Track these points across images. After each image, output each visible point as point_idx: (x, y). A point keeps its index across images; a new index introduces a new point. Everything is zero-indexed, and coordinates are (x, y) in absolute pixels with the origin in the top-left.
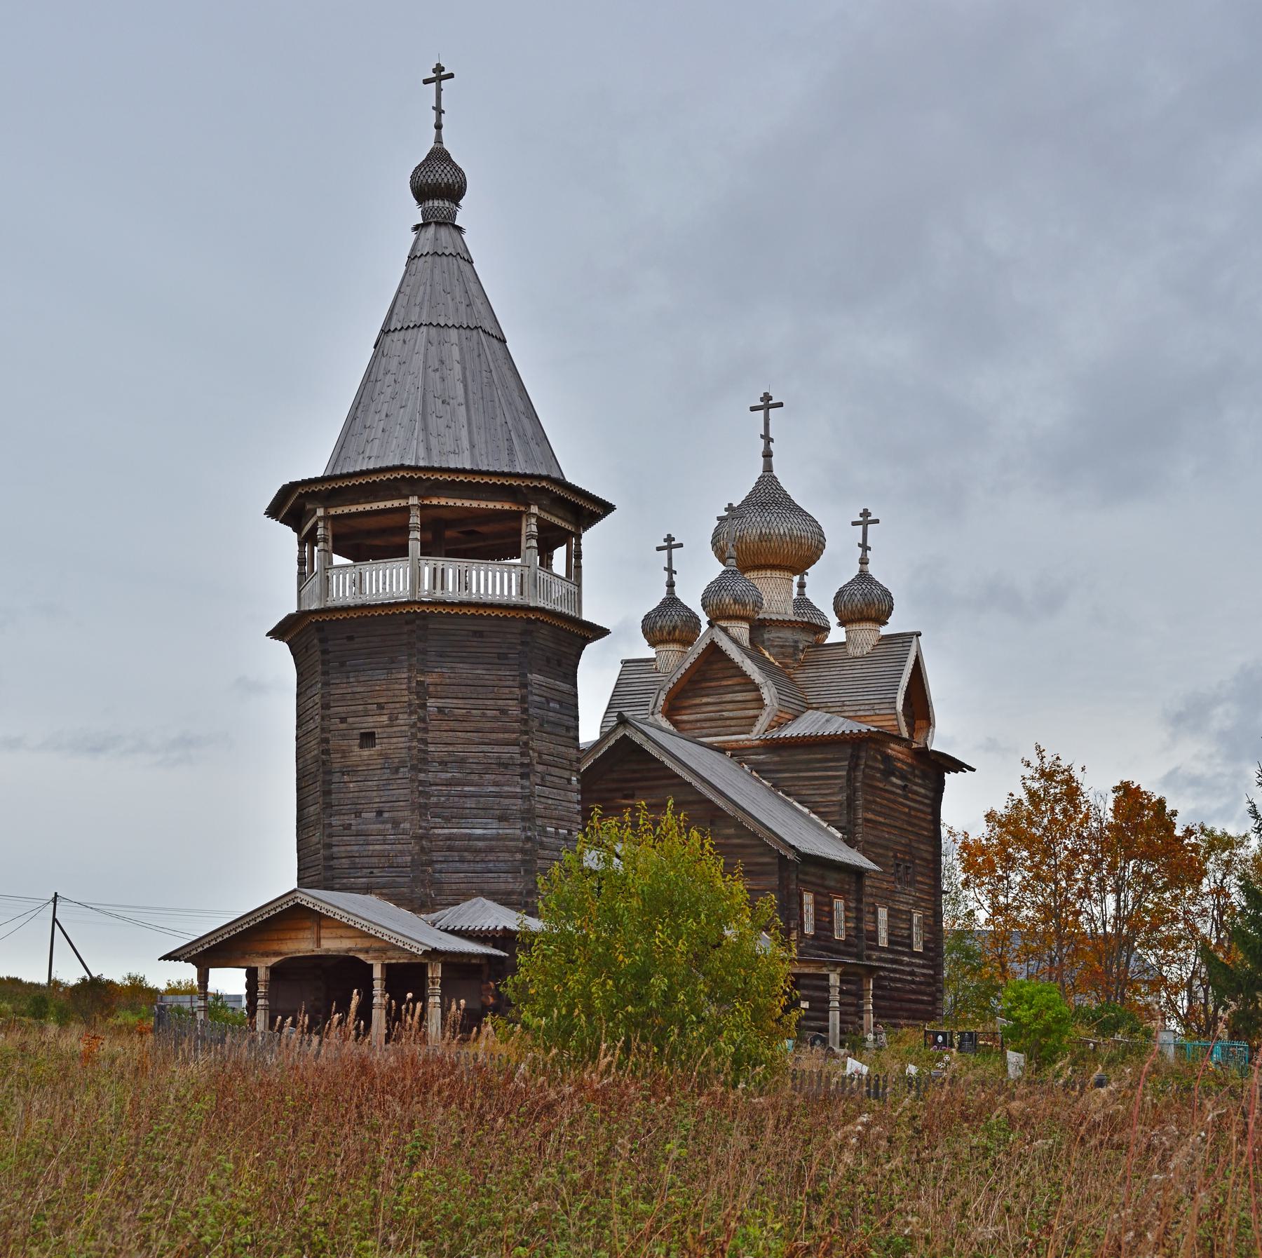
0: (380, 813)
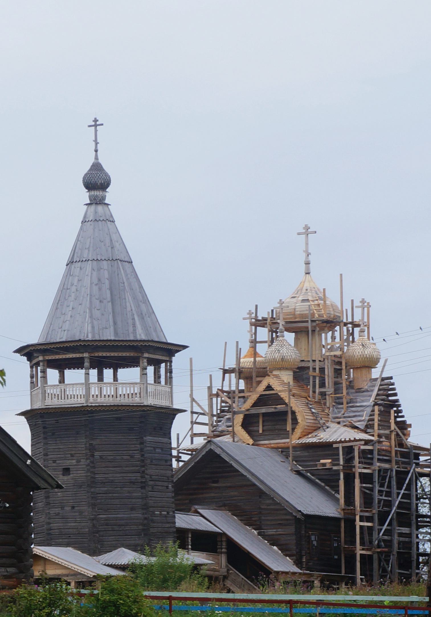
0: (73, 507)
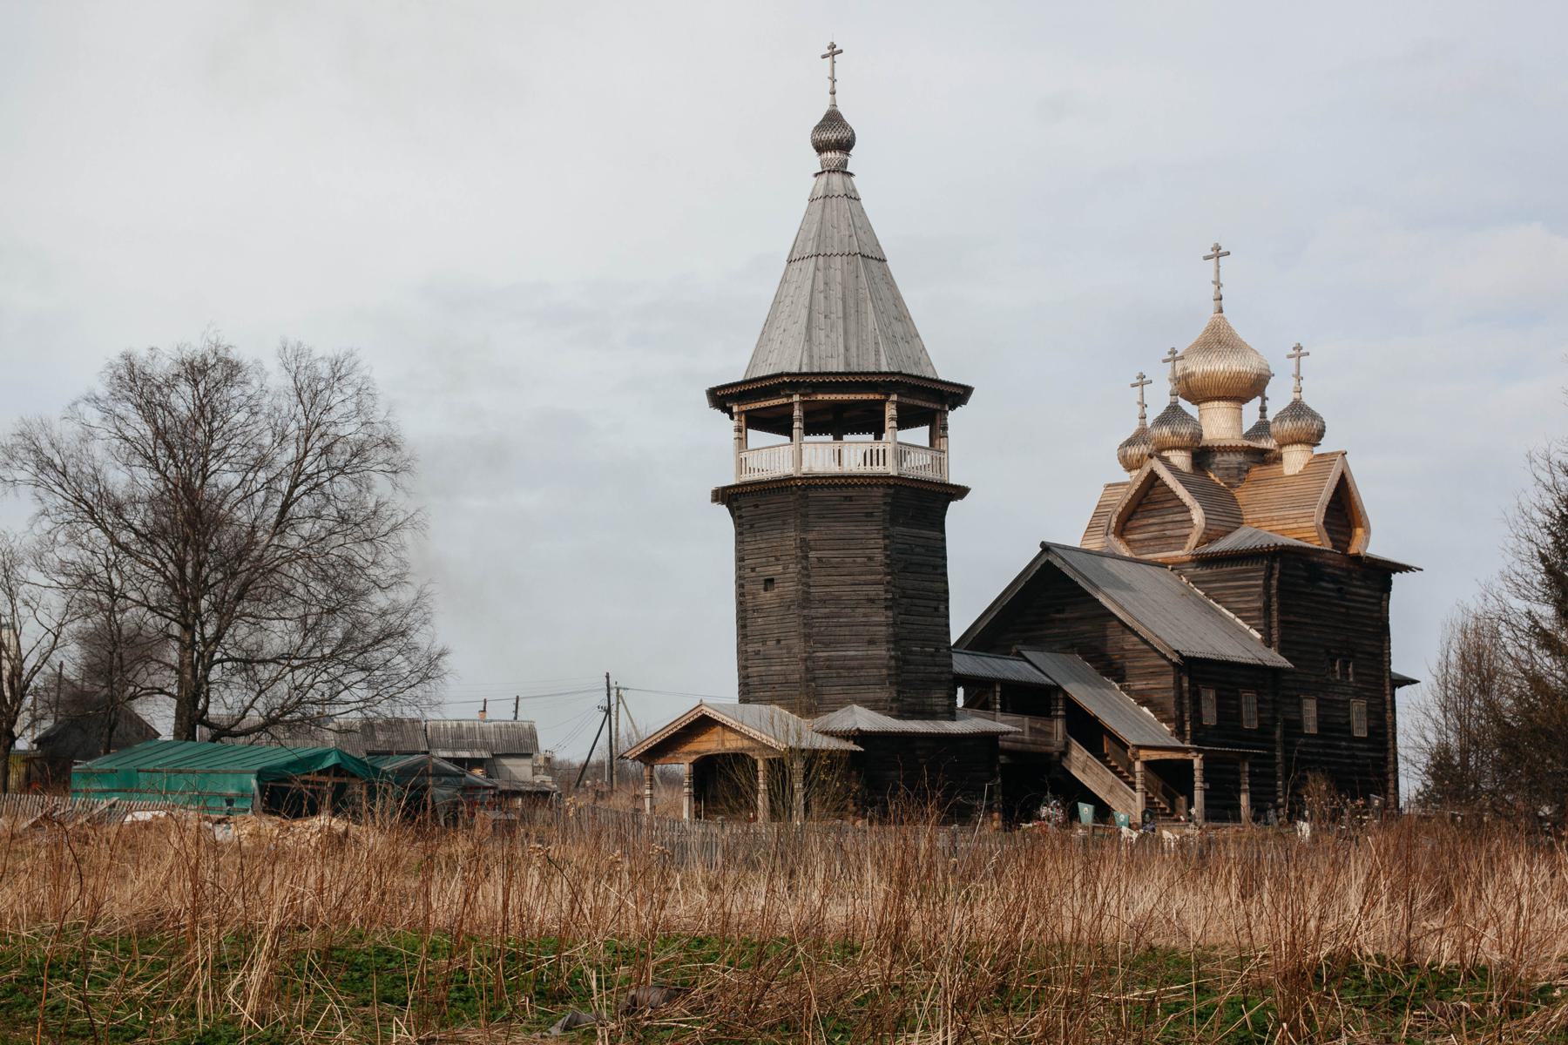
0: (779, 641)
